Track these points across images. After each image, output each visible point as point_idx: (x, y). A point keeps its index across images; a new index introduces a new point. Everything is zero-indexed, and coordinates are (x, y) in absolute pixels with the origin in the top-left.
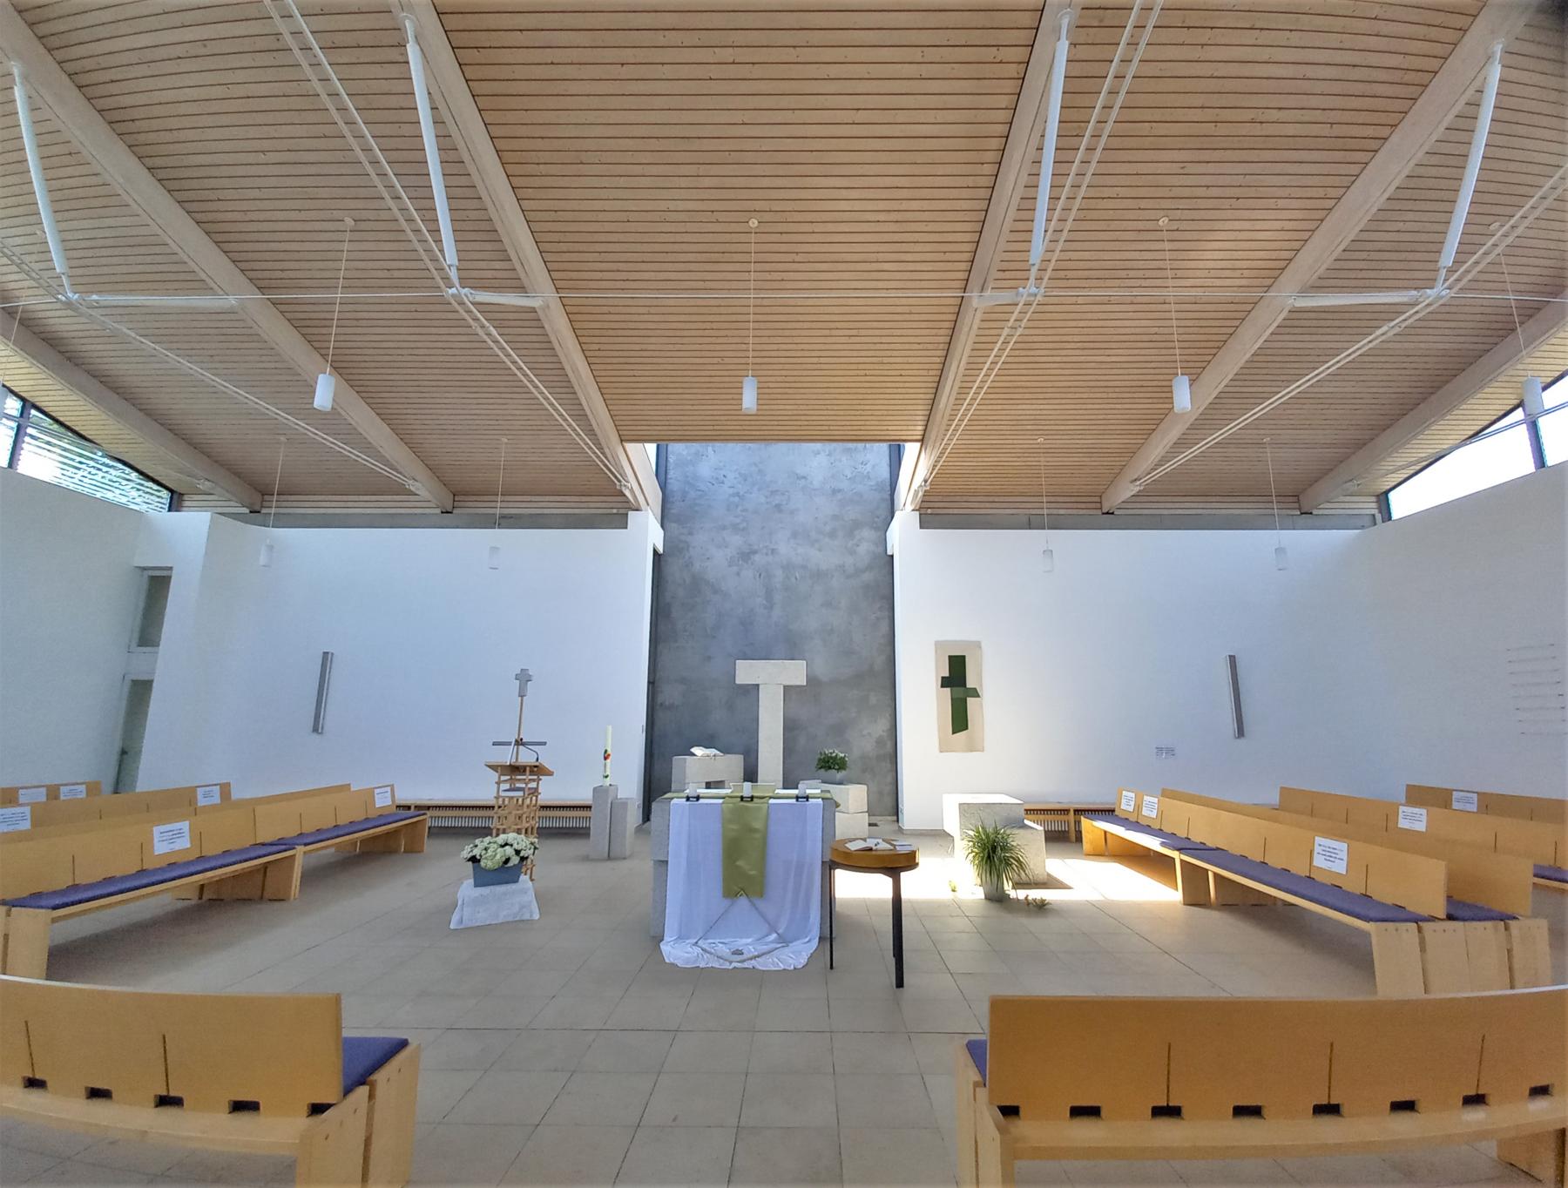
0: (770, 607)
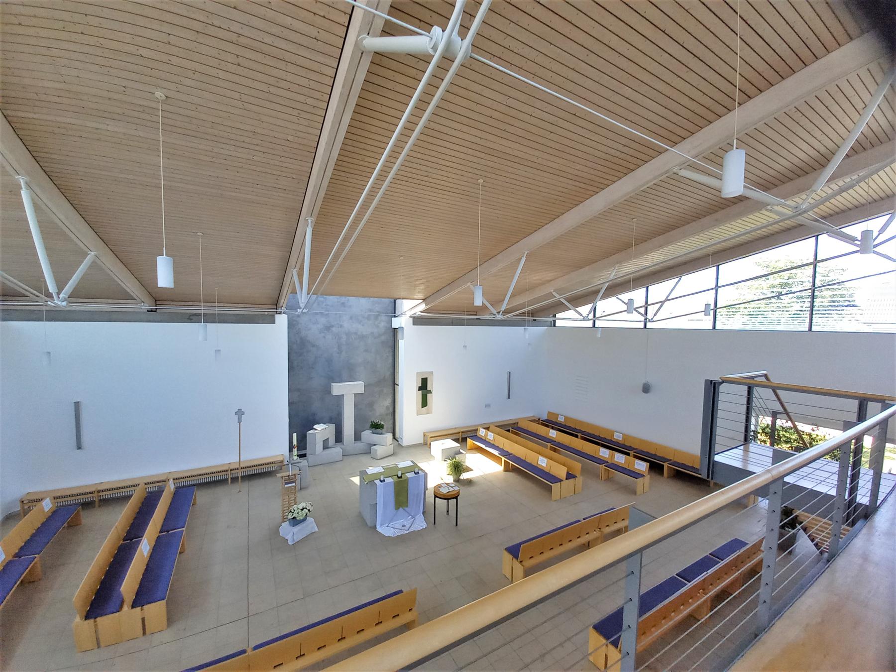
0: (340, 352)
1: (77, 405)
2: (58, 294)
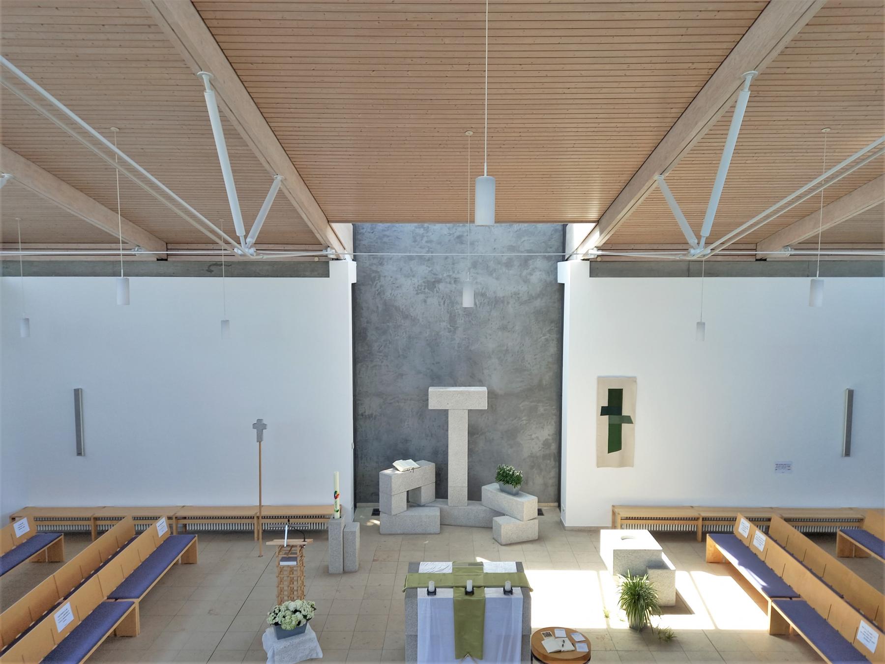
0: (453, 328)
1: (77, 393)
2: (246, 237)
